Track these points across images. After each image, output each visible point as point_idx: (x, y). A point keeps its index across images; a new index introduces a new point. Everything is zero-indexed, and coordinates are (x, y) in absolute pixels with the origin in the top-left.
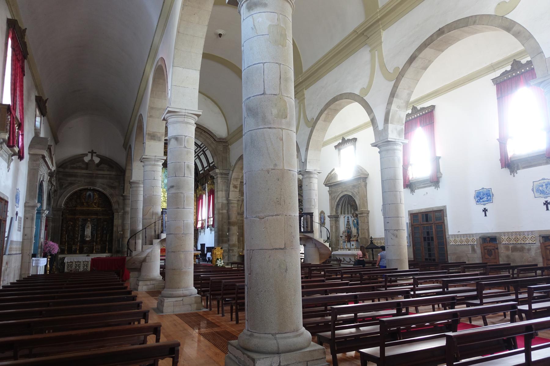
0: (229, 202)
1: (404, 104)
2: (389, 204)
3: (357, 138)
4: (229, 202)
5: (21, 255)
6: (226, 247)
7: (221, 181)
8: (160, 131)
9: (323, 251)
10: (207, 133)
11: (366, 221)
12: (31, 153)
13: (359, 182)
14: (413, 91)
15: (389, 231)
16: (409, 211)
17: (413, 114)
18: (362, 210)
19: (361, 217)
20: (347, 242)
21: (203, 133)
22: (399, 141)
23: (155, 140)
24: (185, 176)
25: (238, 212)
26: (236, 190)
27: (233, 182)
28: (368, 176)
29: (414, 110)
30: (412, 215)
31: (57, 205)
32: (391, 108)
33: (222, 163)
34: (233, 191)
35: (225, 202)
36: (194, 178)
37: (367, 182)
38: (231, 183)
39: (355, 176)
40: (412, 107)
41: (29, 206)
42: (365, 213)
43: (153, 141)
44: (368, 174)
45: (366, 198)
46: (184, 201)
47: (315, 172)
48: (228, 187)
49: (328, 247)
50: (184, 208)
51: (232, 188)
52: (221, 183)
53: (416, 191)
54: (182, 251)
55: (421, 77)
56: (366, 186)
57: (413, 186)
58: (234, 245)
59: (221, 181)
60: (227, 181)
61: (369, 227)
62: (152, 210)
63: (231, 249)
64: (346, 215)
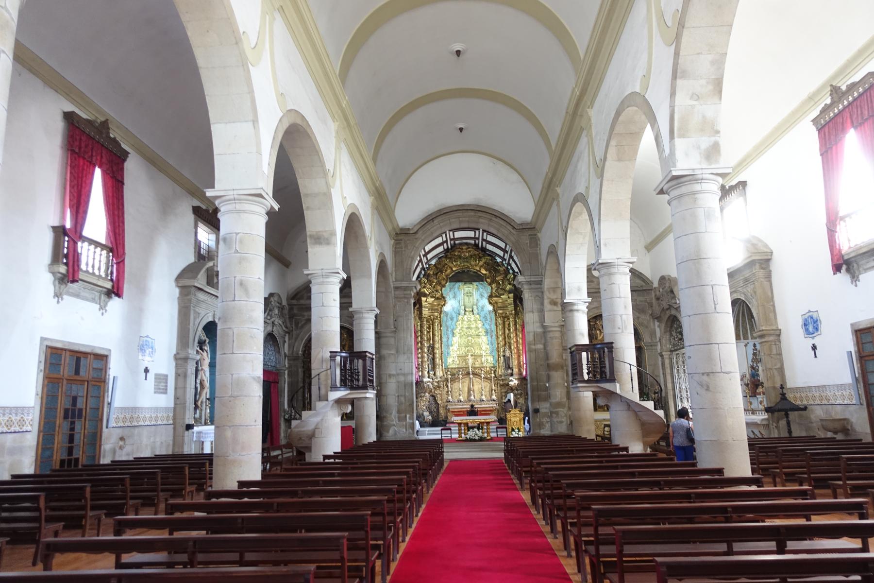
0: (545, 330)
1: (711, 87)
2: (689, 316)
3: (746, 182)
4: (545, 330)
5: (173, 426)
6: (546, 408)
7: (530, 295)
8: (327, 229)
9: (645, 418)
10: (500, 218)
11: (774, 352)
12: (180, 285)
13: (754, 271)
14: (726, 54)
15: (692, 377)
16: (852, 325)
17: (836, 104)
18: (764, 328)
19: (764, 344)
20: (750, 396)
21: (494, 219)
22: (704, 171)
23: (320, 243)
24: (236, 299)
25: (563, 347)
26: (555, 308)
27: (548, 296)
28: (771, 255)
29: (835, 95)
30: (858, 333)
31: (293, 352)
32: (676, 104)
33: (529, 265)
34: (550, 311)
35: (540, 330)
36: (263, 303)
37: (771, 269)
38: (545, 297)
39: (746, 259)
40: (829, 89)
41: (180, 359)
42: (770, 335)
43: (318, 246)
44: (772, 253)
45: (772, 303)
46: (233, 341)
47: (619, 263)
48: (542, 304)
49: (653, 410)
50: (233, 353)
51: (547, 306)
52: (530, 298)
53: (861, 277)
54: (229, 426)
55: (734, 16)
56: (769, 277)
57: (853, 267)
58: (559, 405)
59: (530, 295)
60: (540, 294)
61: (782, 365)
62: (321, 355)
63: (554, 410)
64: (750, 340)
